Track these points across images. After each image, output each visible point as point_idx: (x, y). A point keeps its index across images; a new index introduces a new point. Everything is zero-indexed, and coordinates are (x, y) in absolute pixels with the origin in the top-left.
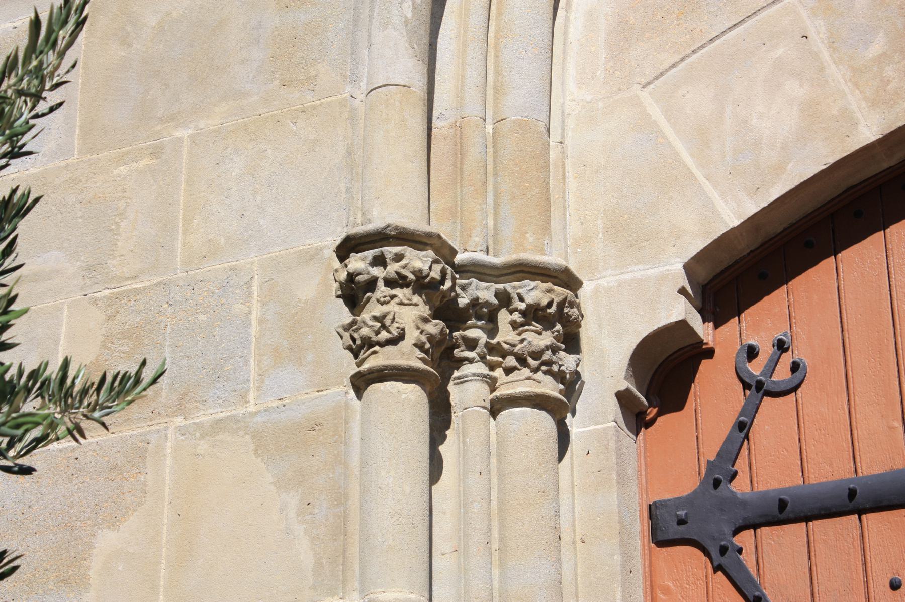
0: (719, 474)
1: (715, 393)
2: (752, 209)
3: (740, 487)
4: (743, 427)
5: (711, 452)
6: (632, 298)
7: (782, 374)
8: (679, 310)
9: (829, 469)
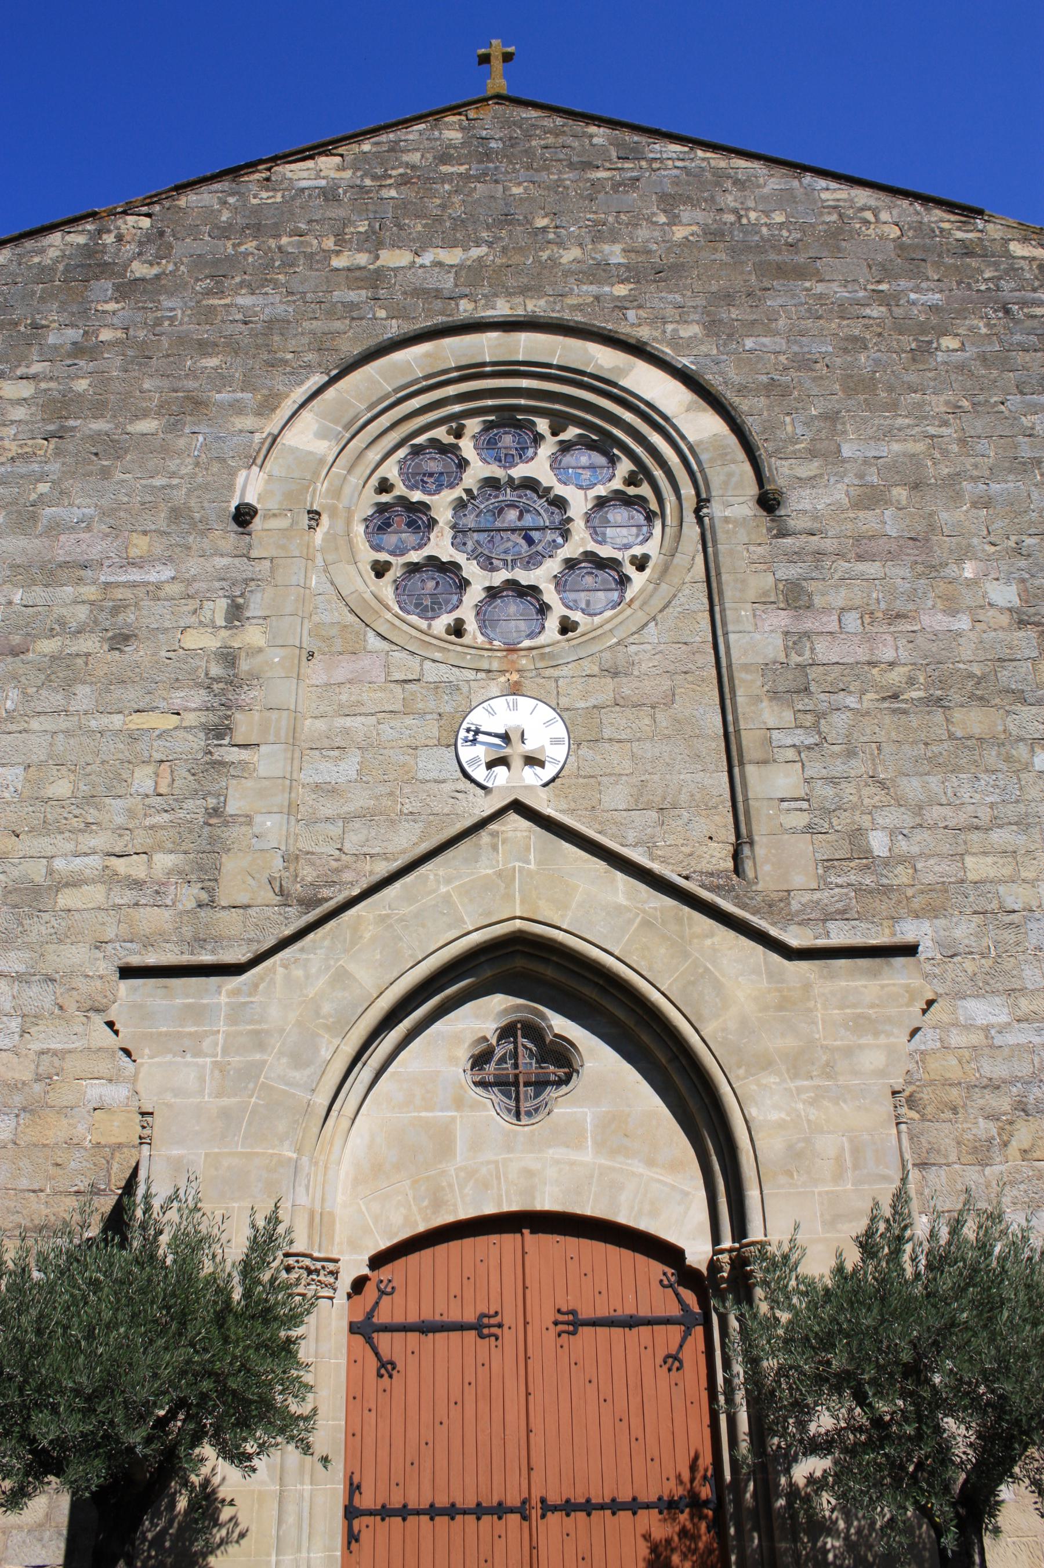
0: (370, 1315)
1: (370, 1290)
2: (389, 1244)
3: (375, 1320)
4: (377, 1303)
5: (368, 1309)
6: (354, 1265)
7: (389, 1289)
8: (366, 1271)
9: (399, 1319)
